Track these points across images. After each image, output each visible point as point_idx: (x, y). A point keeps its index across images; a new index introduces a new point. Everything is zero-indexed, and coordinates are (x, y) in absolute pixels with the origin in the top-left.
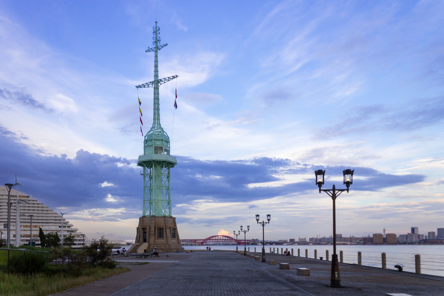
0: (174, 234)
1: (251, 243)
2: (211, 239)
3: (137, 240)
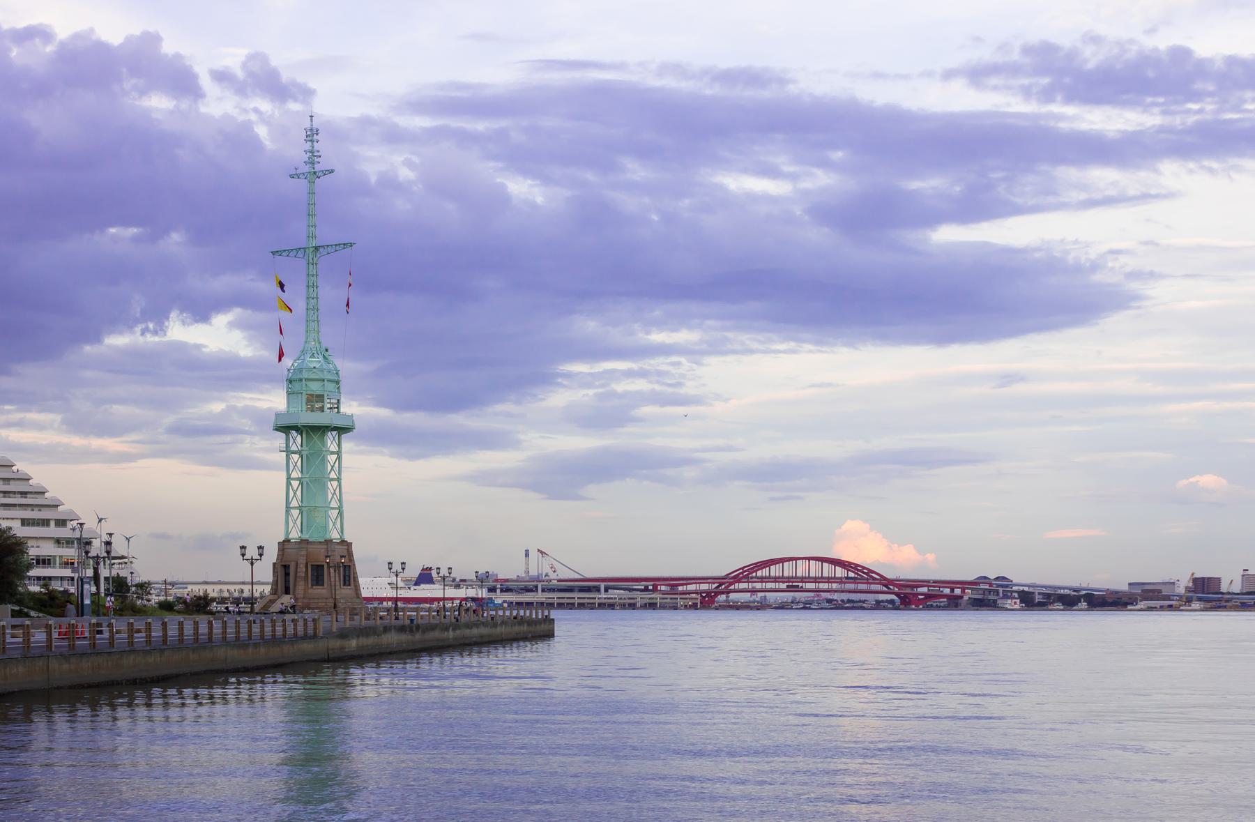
0: (347, 578)
1: (966, 598)
2: (759, 573)
3: (274, 591)
